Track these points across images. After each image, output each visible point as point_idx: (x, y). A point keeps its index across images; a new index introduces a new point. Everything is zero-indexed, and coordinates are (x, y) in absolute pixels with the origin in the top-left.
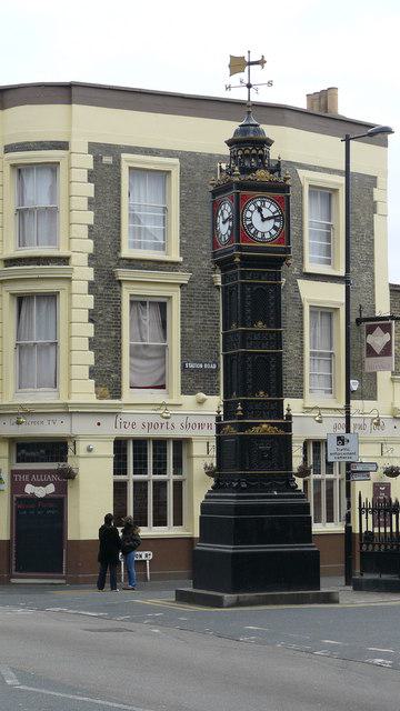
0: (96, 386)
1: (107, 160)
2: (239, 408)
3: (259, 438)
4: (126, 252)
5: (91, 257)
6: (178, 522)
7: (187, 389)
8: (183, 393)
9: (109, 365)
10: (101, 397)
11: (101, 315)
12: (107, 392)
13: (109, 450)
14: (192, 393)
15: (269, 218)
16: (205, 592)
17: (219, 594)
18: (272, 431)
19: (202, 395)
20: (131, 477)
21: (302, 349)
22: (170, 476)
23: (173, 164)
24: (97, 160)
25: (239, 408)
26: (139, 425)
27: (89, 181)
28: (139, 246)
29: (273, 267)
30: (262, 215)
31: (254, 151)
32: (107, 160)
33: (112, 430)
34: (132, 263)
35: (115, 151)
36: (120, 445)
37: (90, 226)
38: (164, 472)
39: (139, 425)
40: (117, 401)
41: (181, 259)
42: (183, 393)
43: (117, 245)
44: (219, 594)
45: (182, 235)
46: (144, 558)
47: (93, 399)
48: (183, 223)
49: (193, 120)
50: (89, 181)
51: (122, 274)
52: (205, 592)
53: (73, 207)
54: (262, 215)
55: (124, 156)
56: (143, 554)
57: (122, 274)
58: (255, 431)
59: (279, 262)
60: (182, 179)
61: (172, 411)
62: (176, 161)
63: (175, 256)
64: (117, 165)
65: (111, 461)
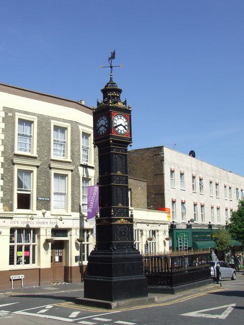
0: (3, 206)
1: (10, 114)
2: (112, 211)
3: (120, 225)
4: (17, 152)
5: (3, 153)
6: (34, 262)
7: (38, 208)
8: (37, 209)
9: (9, 197)
10: (5, 211)
11: (6, 177)
12: (7, 208)
13: (8, 232)
14: (40, 209)
15: (119, 125)
16: (95, 300)
17: (86, 299)
18: (125, 222)
19: (44, 211)
20: (31, 243)
21: (79, 193)
22: (31, 243)
23: (35, 120)
24: (6, 114)
25: (112, 211)
26: (20, 222)
27: (3, 122)
28: (21, 149)
29: (124, 146)
30: (122, 126)
31: (115, 94)
32: (10, 114)
33: (10, 224)
34: (18, 156)
35: (13, 111)
36: (12, 230)
37: (3, 140)
38: (13, 242)
39: (20, 222)
40: (11, 212)
41: (37, 156)
42: (37, 209)
43: (13, 149)
44: (86, 299)
45: (38, 146)
46: (21, 278)
47: (2, 211)
48: (38, 142)
49: (45, 103)
50: (3, 122)
51: (16, 160)
52: (95, 300)
53: (113, 65)
54: (122, 126)
55: (16, 113)
56: (21, 276)
57: (16, 160)
58: (119, 222)
59: (128, 143)
60: (38, 125)
61: (34, 216)
62: (36, 117)
63: (35, 155)
64: (13, 117)
65: (9, 237)
